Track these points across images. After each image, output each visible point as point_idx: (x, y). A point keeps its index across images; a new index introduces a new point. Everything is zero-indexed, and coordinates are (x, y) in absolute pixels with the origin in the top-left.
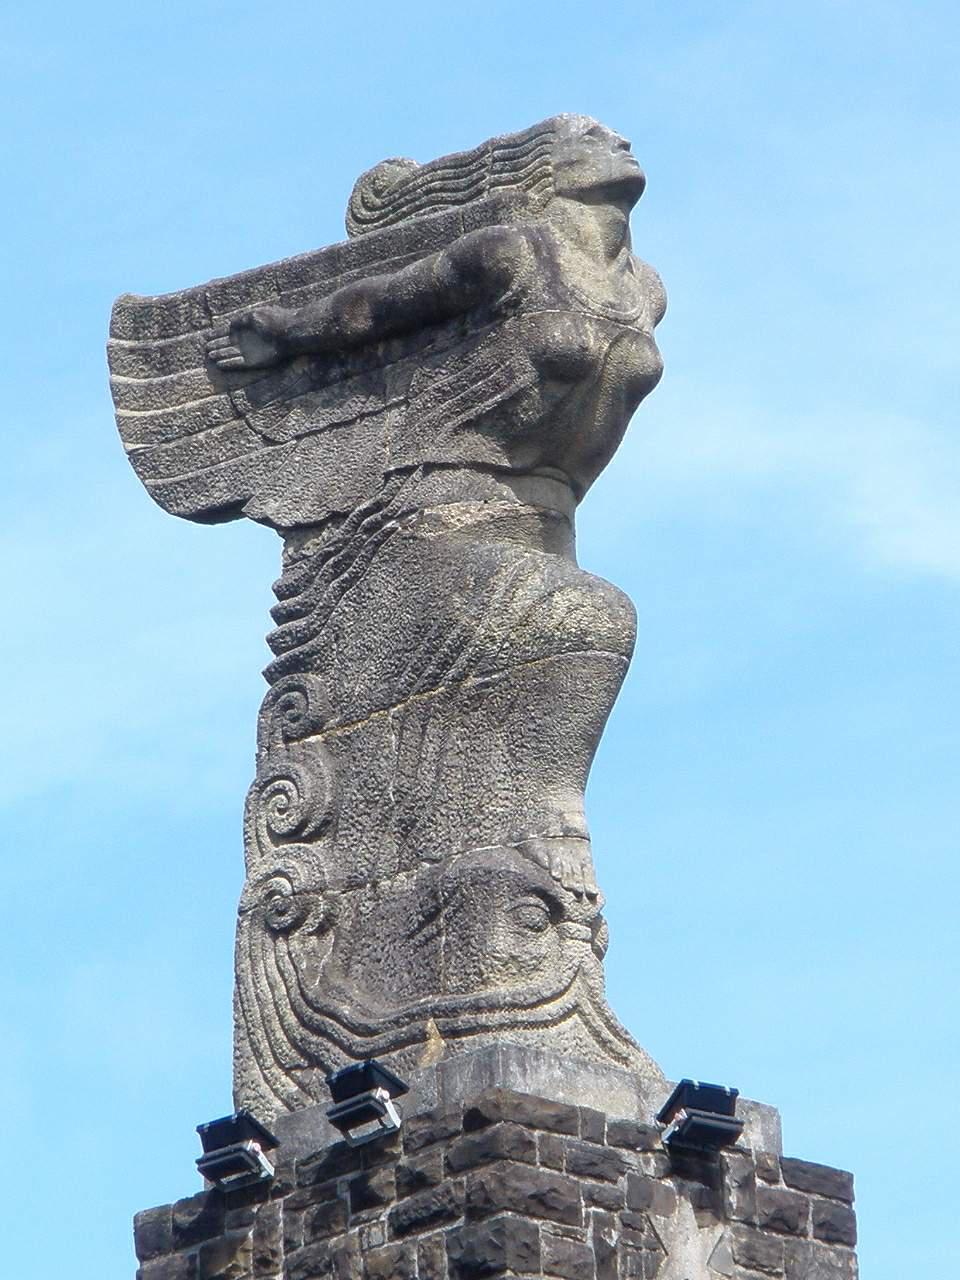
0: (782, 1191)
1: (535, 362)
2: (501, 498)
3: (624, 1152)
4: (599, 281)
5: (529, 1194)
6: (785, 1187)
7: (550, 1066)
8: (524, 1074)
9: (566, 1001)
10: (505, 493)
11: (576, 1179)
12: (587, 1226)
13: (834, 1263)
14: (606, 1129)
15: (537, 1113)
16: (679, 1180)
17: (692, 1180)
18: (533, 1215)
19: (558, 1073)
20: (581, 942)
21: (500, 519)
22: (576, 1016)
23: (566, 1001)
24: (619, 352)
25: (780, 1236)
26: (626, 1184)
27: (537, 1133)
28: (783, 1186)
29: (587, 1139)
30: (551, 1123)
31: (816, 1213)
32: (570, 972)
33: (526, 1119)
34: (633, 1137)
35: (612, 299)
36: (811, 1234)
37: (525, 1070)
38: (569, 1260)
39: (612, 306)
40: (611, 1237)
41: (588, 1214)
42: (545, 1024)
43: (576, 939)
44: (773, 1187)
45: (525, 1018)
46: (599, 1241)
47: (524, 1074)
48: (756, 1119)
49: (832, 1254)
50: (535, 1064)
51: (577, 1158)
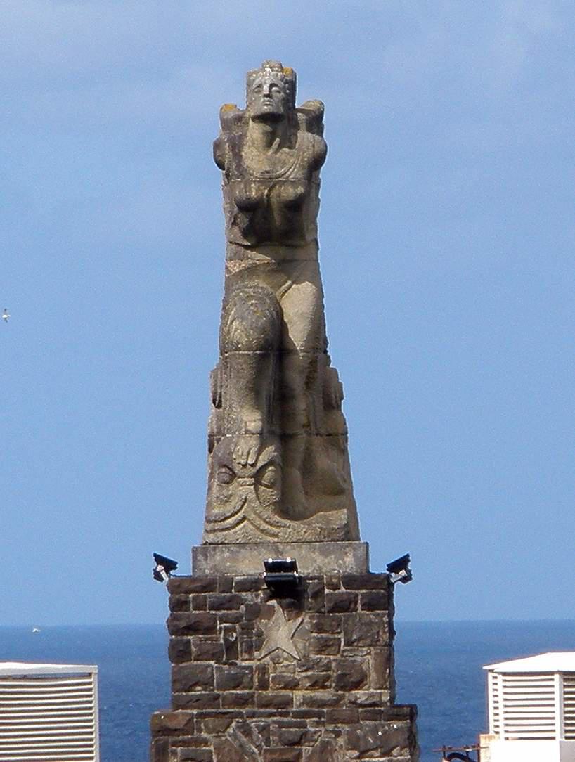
0: (343, 593)
1: (237, 205)
2: (248, 258)
3: (244, 594)
4: (260, 161)
5: (182, 626)
6: (344, 590)
7: (223, 552)
8: (206, 560)
9: (240, 515)
10: (249, 256)
11: (214, 612)
12: (220, 633)
13: (373, 620)
14: (234, 584)
15: (190, 587)
16: (278, 600)
17: (285, 598)
18: (187, 635)
19: (227, 554)
20: (248, 487)
21: (248, 268)
22: (245, 522)
23: (240, 515)
24: (275, 192)
25: (340, 614)
26: (244, 609)
27: (191, 596)
28: (343, 590)
29: (223, 592)
30: (197, 590)
31: (362, 599)
32: (240, 503)
33: (183, 590)
34: (251, 585)
35: (268, 169)
36: (360, 609)
37: (207, 557)
38: (208, 651)
39: (267, 172)
40: (233, 636)
41: (221, 628)
42: (228, 529)
43: (245, 485)
44: (337, 591)
45: (218, 527)
46: (226, 640)
47: (206, 560)
48: (350, 551)
49: (372, 616)
50: (213, 553)
51: (213, 603)
